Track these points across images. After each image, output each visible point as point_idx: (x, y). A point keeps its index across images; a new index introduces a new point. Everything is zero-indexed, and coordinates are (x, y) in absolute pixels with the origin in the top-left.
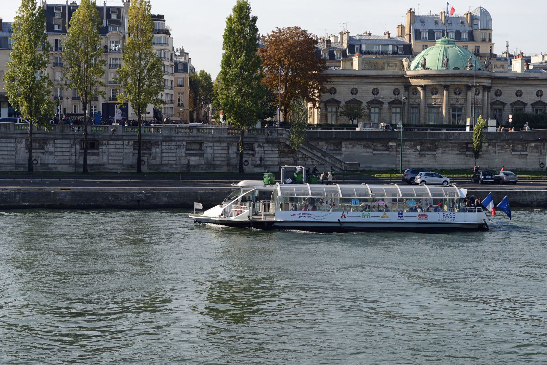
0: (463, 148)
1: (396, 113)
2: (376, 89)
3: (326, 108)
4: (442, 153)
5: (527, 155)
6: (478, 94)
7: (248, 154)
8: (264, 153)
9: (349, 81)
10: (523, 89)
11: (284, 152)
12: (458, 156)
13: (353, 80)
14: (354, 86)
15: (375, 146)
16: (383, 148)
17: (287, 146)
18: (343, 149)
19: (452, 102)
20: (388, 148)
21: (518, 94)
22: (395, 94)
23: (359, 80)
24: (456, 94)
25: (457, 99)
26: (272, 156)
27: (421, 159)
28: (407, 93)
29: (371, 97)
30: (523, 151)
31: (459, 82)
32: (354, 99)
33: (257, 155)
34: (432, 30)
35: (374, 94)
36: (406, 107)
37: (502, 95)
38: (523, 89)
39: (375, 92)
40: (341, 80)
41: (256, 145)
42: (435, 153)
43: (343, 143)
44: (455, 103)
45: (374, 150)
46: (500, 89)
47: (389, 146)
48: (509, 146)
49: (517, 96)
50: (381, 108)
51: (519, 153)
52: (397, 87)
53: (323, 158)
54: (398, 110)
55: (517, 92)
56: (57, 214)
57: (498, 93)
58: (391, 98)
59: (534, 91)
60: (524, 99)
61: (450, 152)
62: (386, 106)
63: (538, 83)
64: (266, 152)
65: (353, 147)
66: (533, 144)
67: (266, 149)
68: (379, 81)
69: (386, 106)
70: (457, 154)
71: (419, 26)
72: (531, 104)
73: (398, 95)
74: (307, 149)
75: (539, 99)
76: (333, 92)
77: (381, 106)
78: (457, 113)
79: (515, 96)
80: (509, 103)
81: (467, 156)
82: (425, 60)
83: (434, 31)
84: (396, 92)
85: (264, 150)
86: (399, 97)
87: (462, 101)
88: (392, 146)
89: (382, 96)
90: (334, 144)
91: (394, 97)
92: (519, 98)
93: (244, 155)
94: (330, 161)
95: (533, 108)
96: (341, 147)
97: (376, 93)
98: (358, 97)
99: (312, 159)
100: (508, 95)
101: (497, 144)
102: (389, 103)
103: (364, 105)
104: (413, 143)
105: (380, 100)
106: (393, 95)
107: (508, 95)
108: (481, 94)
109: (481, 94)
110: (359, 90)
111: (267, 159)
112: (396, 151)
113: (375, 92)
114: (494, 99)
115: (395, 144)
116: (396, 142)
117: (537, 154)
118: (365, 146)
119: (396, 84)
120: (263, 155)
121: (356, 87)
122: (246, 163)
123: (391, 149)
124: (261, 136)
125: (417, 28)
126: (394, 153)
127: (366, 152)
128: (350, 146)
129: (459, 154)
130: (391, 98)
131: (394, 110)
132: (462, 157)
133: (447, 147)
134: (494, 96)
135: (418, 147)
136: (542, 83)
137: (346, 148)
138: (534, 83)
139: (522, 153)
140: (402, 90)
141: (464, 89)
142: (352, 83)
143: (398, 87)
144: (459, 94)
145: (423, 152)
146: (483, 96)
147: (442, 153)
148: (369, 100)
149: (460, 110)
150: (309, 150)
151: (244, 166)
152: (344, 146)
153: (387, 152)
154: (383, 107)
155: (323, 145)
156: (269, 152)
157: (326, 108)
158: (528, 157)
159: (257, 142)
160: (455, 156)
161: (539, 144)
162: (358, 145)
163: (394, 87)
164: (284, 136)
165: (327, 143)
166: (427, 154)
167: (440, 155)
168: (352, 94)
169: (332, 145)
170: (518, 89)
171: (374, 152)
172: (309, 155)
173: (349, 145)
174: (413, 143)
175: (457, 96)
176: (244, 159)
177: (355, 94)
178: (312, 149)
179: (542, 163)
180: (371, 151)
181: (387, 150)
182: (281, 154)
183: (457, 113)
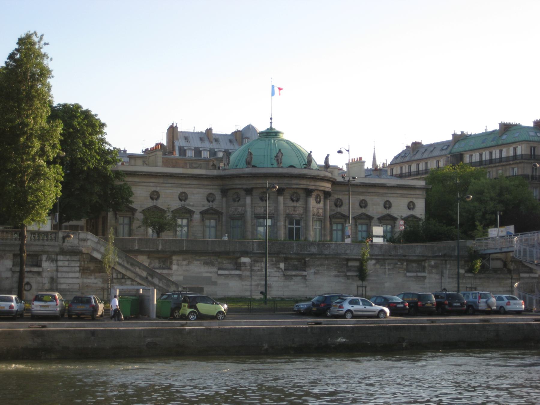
1: (209, 227)
2: (184, 193)
3: (116, 218)
4: (315, 273)
5: (424, 277)
6: (319, 202)
7: (30, 272)
8: (57, 271)
10: (368, 198)
11: (88, 269)
13: (153, 180)
14: (155, 189)
15: (219, 263)
16: (231, 266)
17: (93, 259)
18: (174, 267)
19: (288, 211)
20: (238, 266)
21: (363, 205)
22: (208, 201)
23: (161, 180)
24: (293, 200)
25: (295, 207)
26: (71, 275)
28: (224, 199)
29: (176, 204)
30: (420, 272)
31: (297, 184)
33: (45, 274)
35: (181, 200)
36: (224, 219)
38: (368, 198)
39: (183, 197)
40: (137, 179)
41: (44, 257)
42: (305, 273)
43: (174, 258)
44: (292, 212)
45: (219, 269)
46: (341, 197)
47: (240, 263)
48: (402, 264)
49: (361, 207)
50: (190, 220)
51: (415, 274)
52: (211, 191)
53: (150, 278)
54: (213, 222)
56: (186, 362)
57: (338, 203)
58: (204, 206)
62: (197, 217)
64: (60, 269)
65: (189, 264)
66: (433, 263)
67: (60, 263)
68: (188, 182)
69: (197, 217)
70: (336, 276)
71: (180, 143)
73: (212, 202)
74: (126, 265)
75: (387, 212)
77: (191, 217)
78: (294, 226)
79: (359, 207)
81: (348, 279)
82: (251, 154)
84: (210, 198)
85: (57, 266)
86: (215, 205)
87: (300, 211)
88: (244, 263)
89: (191, 203)
90: (159, 258)
91: (207, 205)
92: (364, 211)
93: (26, 274)
94: (161, 285)
96: (171, 263)
97: (184, 198)
98: (160, 203)
99: (133, 280)
101: (387, 262)
102: (201, 213)
103: (169, 215)
104: (274, 259)
105: (190, 208)
106: (206, 202)
108: (322, 202)
109: (322, 202)
110: (162, 194)
111: (62, 281)
112: (252, 270)
113: (183, 197)
114: (334, 210)
115: (250, 261)
116: (250, 257)
117: (437, 277)
118: (206, 263)
120: (55, 273)
121: (158, 189)
122: (27, 287)
123: (243, 268)
124: (52, 243)
126: (248, 273)
127: (207, 272)
128: (185, 263)
130: (204, 206)
131: (207, 222)
132: (342, 280)
133: (321, 265)
134: (334, 207)
135: (282, 265)
136: (390, 192)
137: (178, 264)
138: (381, 191)
139: (419, 274)
141: (302, 195)
142: (151, 184)
143: (213, 191)
144: (297, 200)
145: (289, 273)
146: (325, 205)
147: (315, 273)
148: (175, 208)
149: (298, 223)
150: (129, 266)
151: (25, 292)
152: (175, 262)
153: (238, 272)
154: (193, 218)
155: (143, 259)
156: (64, 269)
157: (116, 218)
158: (427, 281)
159: (44, 252)
161: (439, 262)
162: (197, 260)
163: (208, 191)
164: (89, 243)
165: (149, 258)
166: (294, 275)
168: (152, 199)
169: (157, 261)
170: (362, 198)
171: (220, 272)
172: (128, 274)
173: (184, 260)
174: (274, 259)
175: (295, 204)
176: (26, 280)
177: (156, 199)
178: (132, 265)
180: (215, 269)
181: (237, 269)
182: (84, 271)
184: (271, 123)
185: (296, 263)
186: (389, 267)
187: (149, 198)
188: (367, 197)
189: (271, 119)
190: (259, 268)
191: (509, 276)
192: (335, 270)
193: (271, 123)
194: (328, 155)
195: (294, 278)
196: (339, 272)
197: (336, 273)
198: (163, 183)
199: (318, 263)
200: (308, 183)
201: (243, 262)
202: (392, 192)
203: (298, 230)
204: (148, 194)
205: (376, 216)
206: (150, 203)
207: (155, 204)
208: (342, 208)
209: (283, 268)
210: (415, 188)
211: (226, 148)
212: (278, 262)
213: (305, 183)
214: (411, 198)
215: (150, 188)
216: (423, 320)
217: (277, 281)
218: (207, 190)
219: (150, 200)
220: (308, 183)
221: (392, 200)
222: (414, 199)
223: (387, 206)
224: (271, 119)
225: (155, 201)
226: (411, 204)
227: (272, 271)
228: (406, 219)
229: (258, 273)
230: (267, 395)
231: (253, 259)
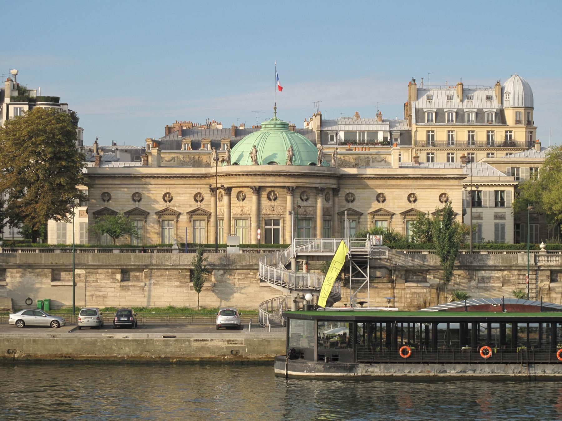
0: (185, 278)
12: (179, 289)
14: (137, 190)
18: (8, 280)
22: (196, 201)
25: (273, 207)
27: (123, 293)
34: (442, 109)
37: (356, 200)
39: (412, 198)
40: (117, 182)
46: (351, 191)
61: (166, 283)
62: (184, 218)
63: (410, 182)
70: (177, 287)
76: (381, 199)
78: (272, 227)
84: (198, 197)
86: (202, 205)
88: (79, 275)
89: (177, 204)
91: (194, 205)
98: (142, 206)
105: (175, 209)
115: (84, 272)
119: (197, 186)
125: (421, 107)
129: (180, 287)
130: (191, 206)
133: (161, 276)
134: (345, 203)
135: (119, 276)
140: (206, 194)
142: (133, 186)
149: (277, 223)
154: (361, 220)
160: (173, 289)
173: (17, 273)
175: (272, 203)
177: (139, 201)
179: (29, 299)
183: (272, 227)
186: (240, 277)
187: (131, 200)
188: (386, 190)
189: (275, 108)
190: (94, 279)
191: (390, 285)
195: (131, 288)
196: (181, 282)
197: (178, 283)
199: (159, 273)
201: (77, 274)
202: (418, 183)
203: (277, 231)
205: (398, 212)
207: (137, 206)
208: (355, 203)
209: (120, 280)
211: (481, 107)
212: (114, 273)
215: (132, 190)
216: (104, 335)
217: (112, 292)
222: (448, 190)
224: (275, 108)
227: (108, 282)
228: (405, 214)
229: (93, 284)
230: (446, 408)
231: (88, 270)
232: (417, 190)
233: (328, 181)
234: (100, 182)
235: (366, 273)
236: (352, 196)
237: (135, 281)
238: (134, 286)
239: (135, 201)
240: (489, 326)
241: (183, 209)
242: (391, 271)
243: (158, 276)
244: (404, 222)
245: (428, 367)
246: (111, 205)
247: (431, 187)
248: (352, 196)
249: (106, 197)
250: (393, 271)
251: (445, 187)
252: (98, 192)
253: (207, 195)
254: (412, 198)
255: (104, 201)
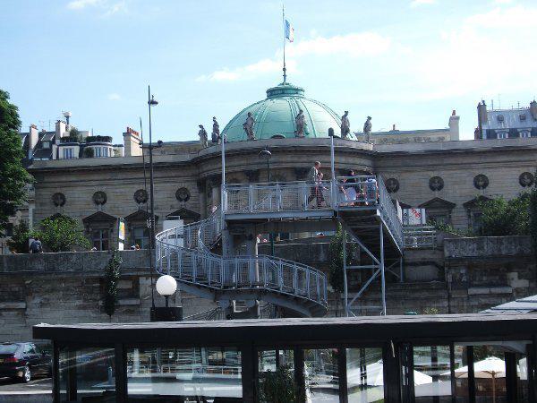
4: (42, 305)
9: (87, 178)
10: (444, 174)
13: (96, 177)
14: (99, 189)
21: (183, 197)
28: (202, 195)
32: (100, 214)
38: (444, 174)
39: (481, 182)
42: (22, 305)
46: (395, 176)
49: (433, 189)
55: (432, 180)
58: (172, 207)
59: (131, 190)
60: (491, 191)
63: (476, 160)
70: (80, 308)
71: (491, 124)
72: (464, 205)
80: (460, 204)
83: (496, 131)
86: (189, 205)
92: (437, 194)
95: (469, 211)
98: (106, 209)
100: (459, 187)
106: (176, 202)
107: (459, 187)
110: (110, 195)
121: (104, 189)
129: (84, 308)
133: (53, 290)
147: (42, 305)
148: (88, 215)
160: (73, 312)
163: (178, 186)
167: (35, 311)
170: (433, 174)
184: (285, 76)
185: (17, 289)
189: (284, 70)
192: (78, 298)
193: (285, 76)
194: (347, 113)
196: (85, 300)
198: (110, 180)
199: (48, 286)
200: (296, 159)
202: (488, 160)
204: (89, 197)
206: (92, 210)
210: (530, 150)
213: (236, 163)
214: (525, 166)
218: (177, 184)
219: (93, 205)
220: (296, 159)
221: (487, 173)
223: (481, 183)
224: (284, 70)
225: (100, 206)
226: (526, 177)
228: (470, 205)
232: (487, 170)
233: (357, 161)
234: (53, 180)
235: (379, 258)
236: (394, 184)
237: (12, 301)
238: (10, 310)
239: (97, 203)
240: (434, 360)
241: (163, 211)
242: (443, 268)
243: (47, 291)
244: (469, 216)
245: (465, 319)
246: (65, 211)
247: (507, 164)
248: (394, 184)
249: (59, 200)
250: (446, 269)
251: (527, 164)
252: (47, 194)
253: (194, 190)
254: (481, 182)
255: (57, 205)
